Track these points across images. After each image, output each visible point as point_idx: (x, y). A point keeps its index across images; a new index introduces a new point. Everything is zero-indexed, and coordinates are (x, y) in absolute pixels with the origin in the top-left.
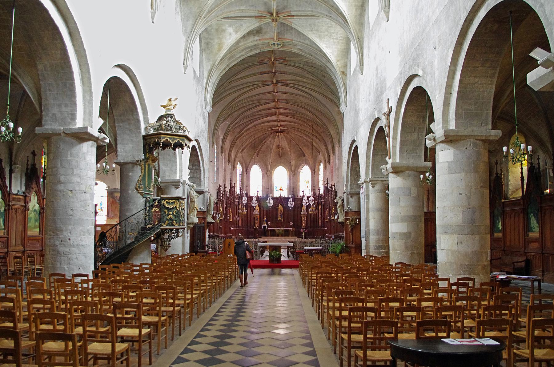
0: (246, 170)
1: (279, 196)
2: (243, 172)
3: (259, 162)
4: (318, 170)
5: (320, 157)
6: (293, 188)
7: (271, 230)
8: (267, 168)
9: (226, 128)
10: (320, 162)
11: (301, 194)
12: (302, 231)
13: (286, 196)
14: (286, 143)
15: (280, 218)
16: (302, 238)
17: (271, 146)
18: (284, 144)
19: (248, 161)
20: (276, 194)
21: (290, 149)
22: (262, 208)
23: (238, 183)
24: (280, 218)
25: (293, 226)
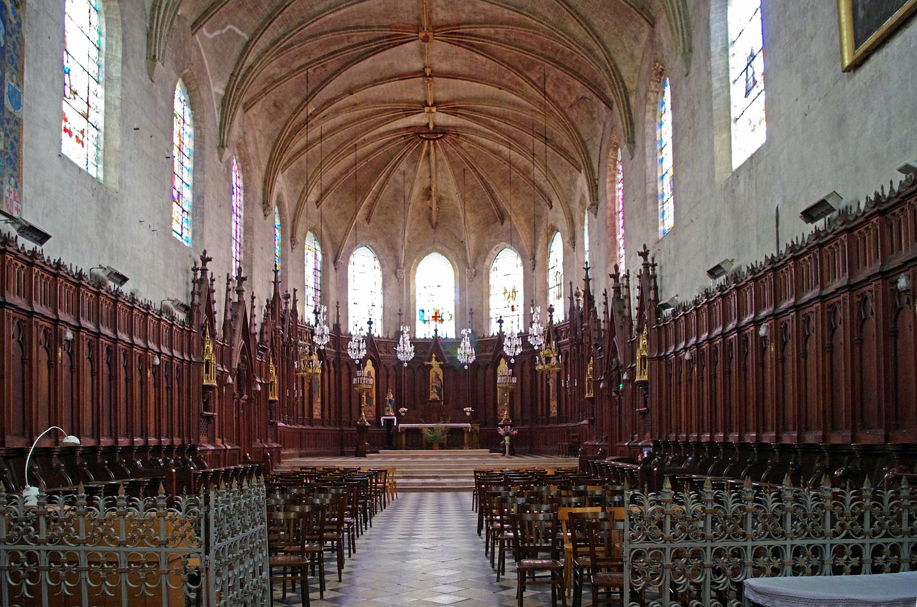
0: (335, 260)
1: (430, 335)
2: (324, 263)
3: (375, 238)
4: (546, 256)
5: (557, 215)
6: (472, 310)
7: (408, 430)
8: (396, 258)
9: (236, 53)
10: (553, 230)
11: (494, 329)
12: (501, 431)
13: (452, 335)
14: (452, 181)
15: (433, 396)
16: (504, 453)
17: (407, 191)
18: (447, 184)
19: (341, 232)
20: (424, 331)
21: (464, 200)
22: (382, 371)
23: (310, 292)
24: (433, 396)
25: (473, 419)
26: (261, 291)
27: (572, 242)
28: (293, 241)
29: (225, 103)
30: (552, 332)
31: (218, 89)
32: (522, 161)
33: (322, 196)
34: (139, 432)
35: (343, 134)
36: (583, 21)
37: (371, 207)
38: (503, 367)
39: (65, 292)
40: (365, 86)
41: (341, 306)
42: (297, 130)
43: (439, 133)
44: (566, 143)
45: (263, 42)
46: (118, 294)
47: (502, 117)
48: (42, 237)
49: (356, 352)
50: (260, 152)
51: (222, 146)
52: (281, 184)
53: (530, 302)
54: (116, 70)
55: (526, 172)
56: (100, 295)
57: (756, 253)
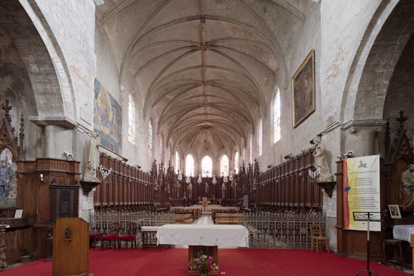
0: (183, 158)
4: (234, 157)
5: (237, 147)
6: (216, 171)
10: (236, 151)
11: (221, 175)
13: (211, 177)
18: (210, 139)
20: (204, 175)
24: (206, 191)
26: (166, 167)
27: (241, 154)
28: (173, 154)
29: (159, 123)
30: (235, 177)
31: (157, 120)
32: (229, 134)
33: (181, 141)
34: (105, 200)
35: (186, 128)
36: (243, 104)
37: (192, 145)
38: (223, 185)
39: (130, 171)
40: (190, 117)
41: (184, 170)
42: (174, 128)
43: (208, 127)
44: (239, 130)
45: (168, 108)
46: (125, 164)
47: (224, 124)
48: (126, 160)
49: (188, 181)
50: (166, 133)
51: (158, 134)
52: (171, 140)
53: (230, 169)
54: (138, 120)
55: (230, 137)
56: (135, 171)
57: (277, 163)
